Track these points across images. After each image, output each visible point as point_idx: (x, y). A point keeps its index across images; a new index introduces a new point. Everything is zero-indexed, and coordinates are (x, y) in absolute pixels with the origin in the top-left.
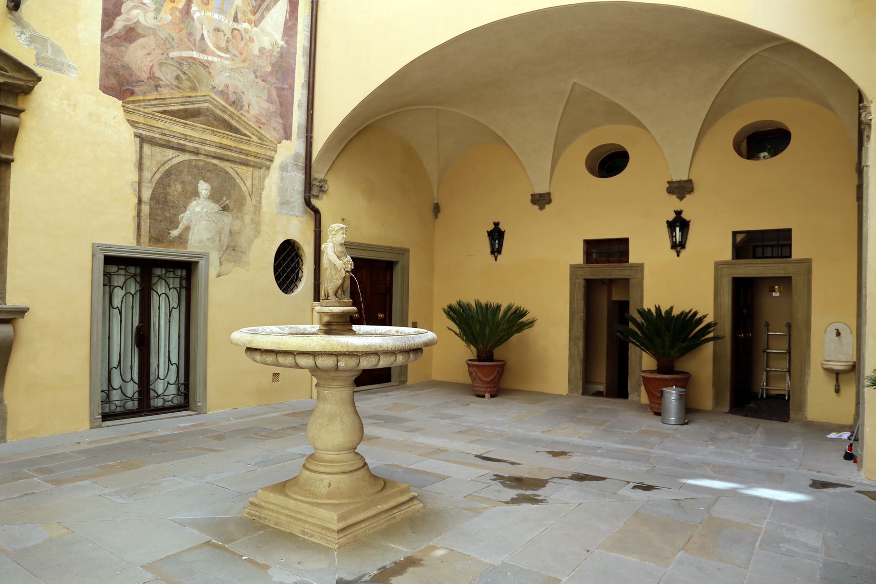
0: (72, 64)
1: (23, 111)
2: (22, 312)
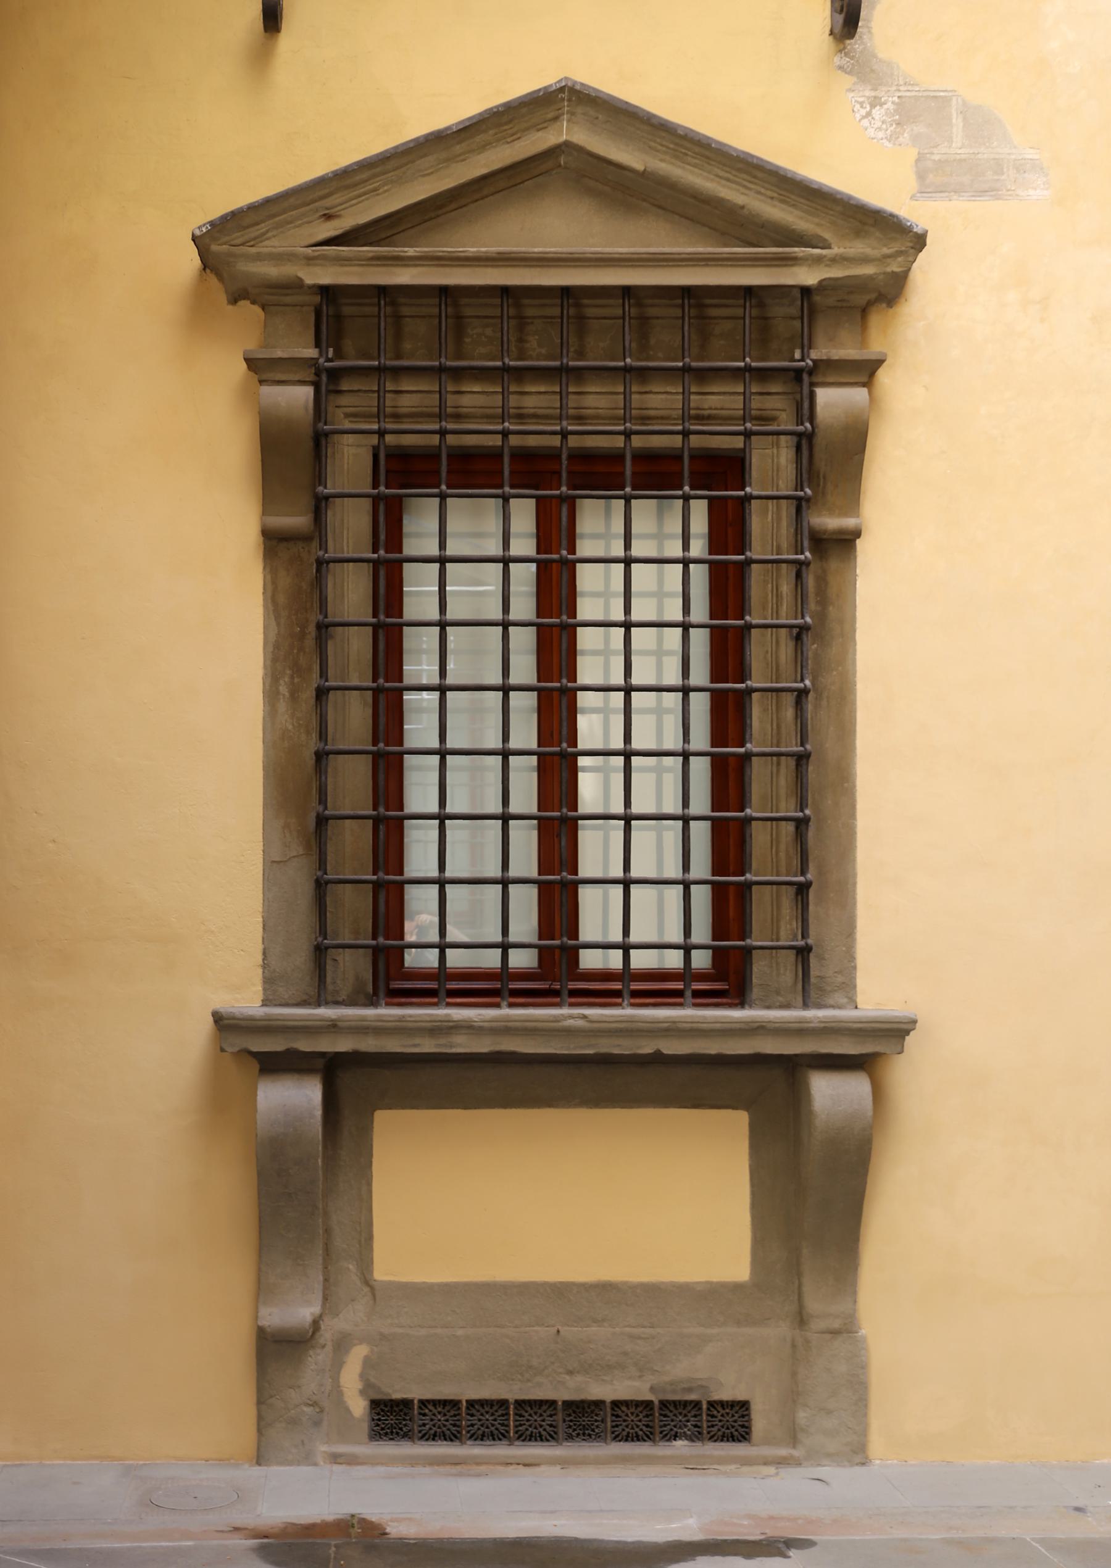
0: (1031, 154)
1: (880, 362)
2: (897, 1032)
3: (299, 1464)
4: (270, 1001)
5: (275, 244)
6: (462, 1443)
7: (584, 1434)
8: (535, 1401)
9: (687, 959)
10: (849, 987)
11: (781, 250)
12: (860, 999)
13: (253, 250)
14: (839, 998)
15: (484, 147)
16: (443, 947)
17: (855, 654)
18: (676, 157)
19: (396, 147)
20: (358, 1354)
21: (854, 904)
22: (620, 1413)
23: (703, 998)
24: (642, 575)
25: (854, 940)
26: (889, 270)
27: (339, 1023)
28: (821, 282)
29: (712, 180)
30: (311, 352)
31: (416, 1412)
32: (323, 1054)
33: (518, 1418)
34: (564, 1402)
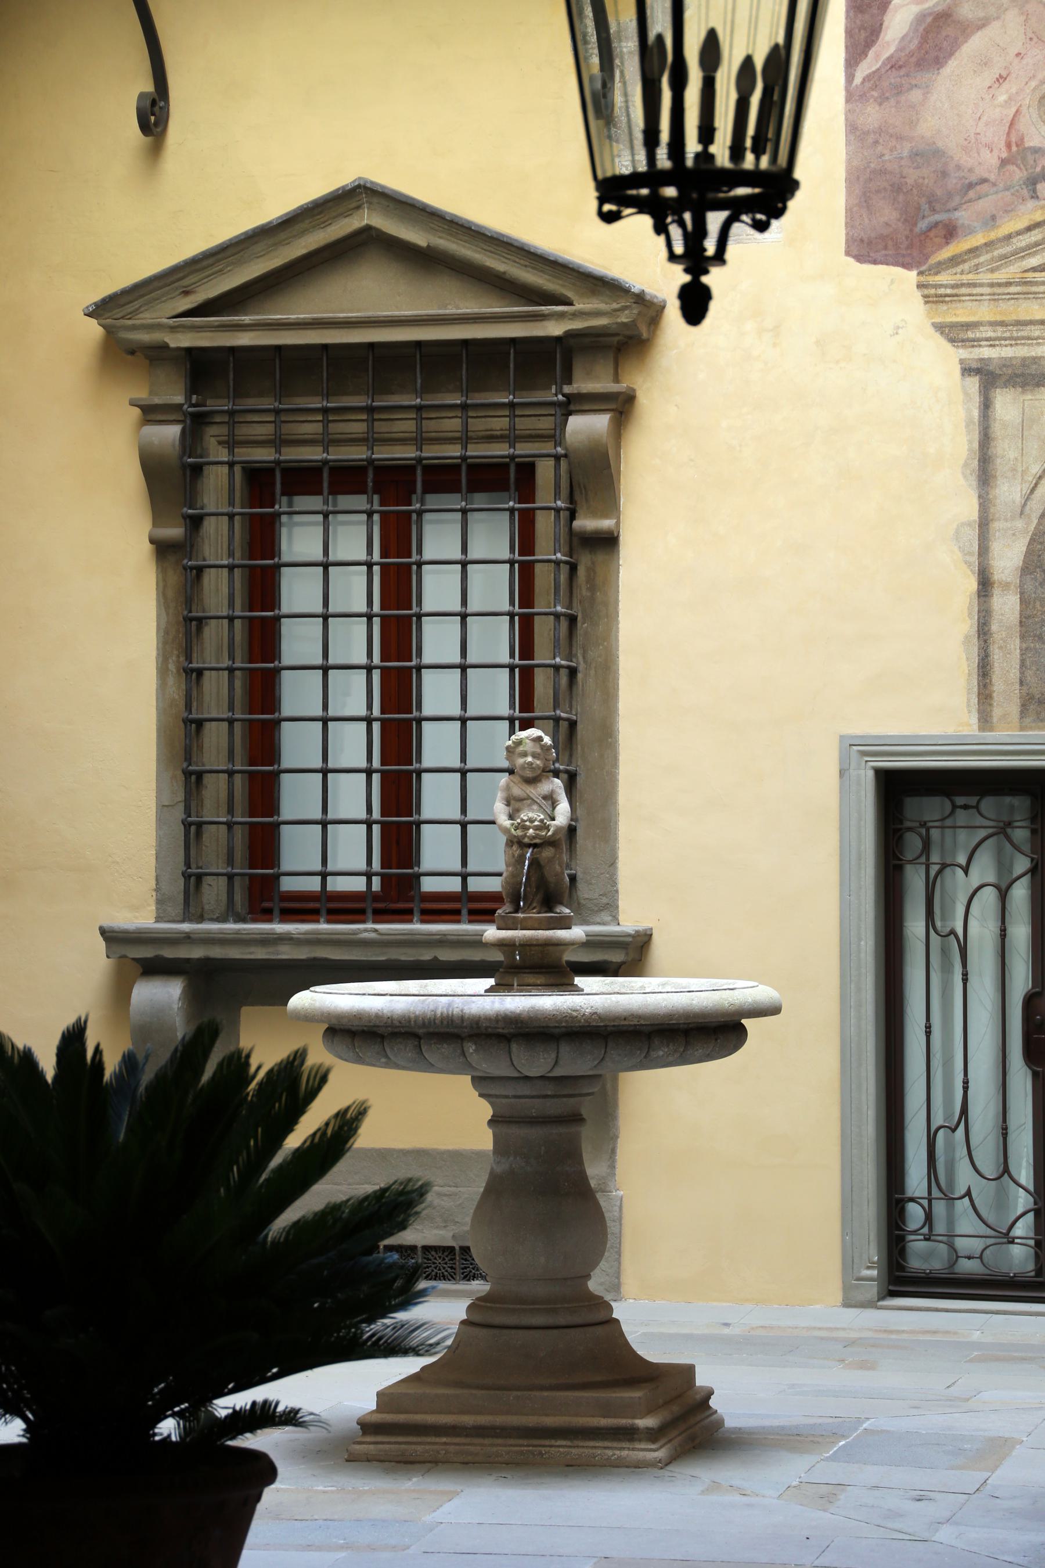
4: (161, 918)
5: (147, 317)
11: (531, 308)
12: (621, 918)
13: (130, 322)
14: (605, 916)
15: (304, 232)
16: (324, 875)
17: (617, 632)
18: (451, 235)
19: (231, 240)
21: (616, 839)
22: (430, 1257)
23: (382, 915)
24: (466, 565)
25: (616, 869)
26: (619, 320)
28: (566, 332)
29: (480, 253)
30: (179, 399)
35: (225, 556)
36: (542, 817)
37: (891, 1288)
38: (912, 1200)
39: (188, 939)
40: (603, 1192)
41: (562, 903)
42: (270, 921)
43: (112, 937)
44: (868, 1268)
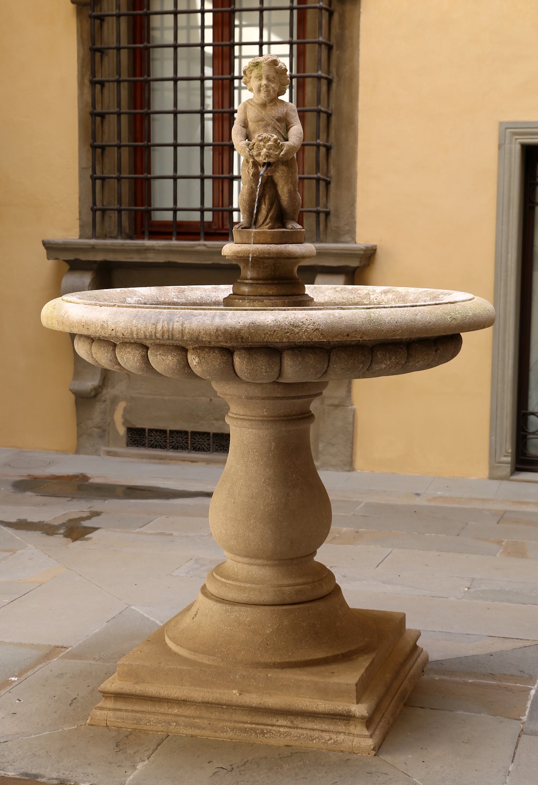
3: (92, 454)
6: (168, 450)
7: (223, 449)
8: (201, 432)
9: (202, 216)
10: (352, 232)
12: (358, 239)
14: (347, 238)
16: (175, 210)
20: (121, 406)
21: (355, 189)
27: (96, 247)
31: (147, 434)
32: (95, 262)
33: (171, 438)
34: (214, 434)
35: (114, 8)
36: (275, 137)
37: (518, 466)
38: (533, 414)
39: (93, 249)
40: (344, 406)
41: (293, 220)
42: (143, 238)
43: (52, 249)
44: (505, 456)
